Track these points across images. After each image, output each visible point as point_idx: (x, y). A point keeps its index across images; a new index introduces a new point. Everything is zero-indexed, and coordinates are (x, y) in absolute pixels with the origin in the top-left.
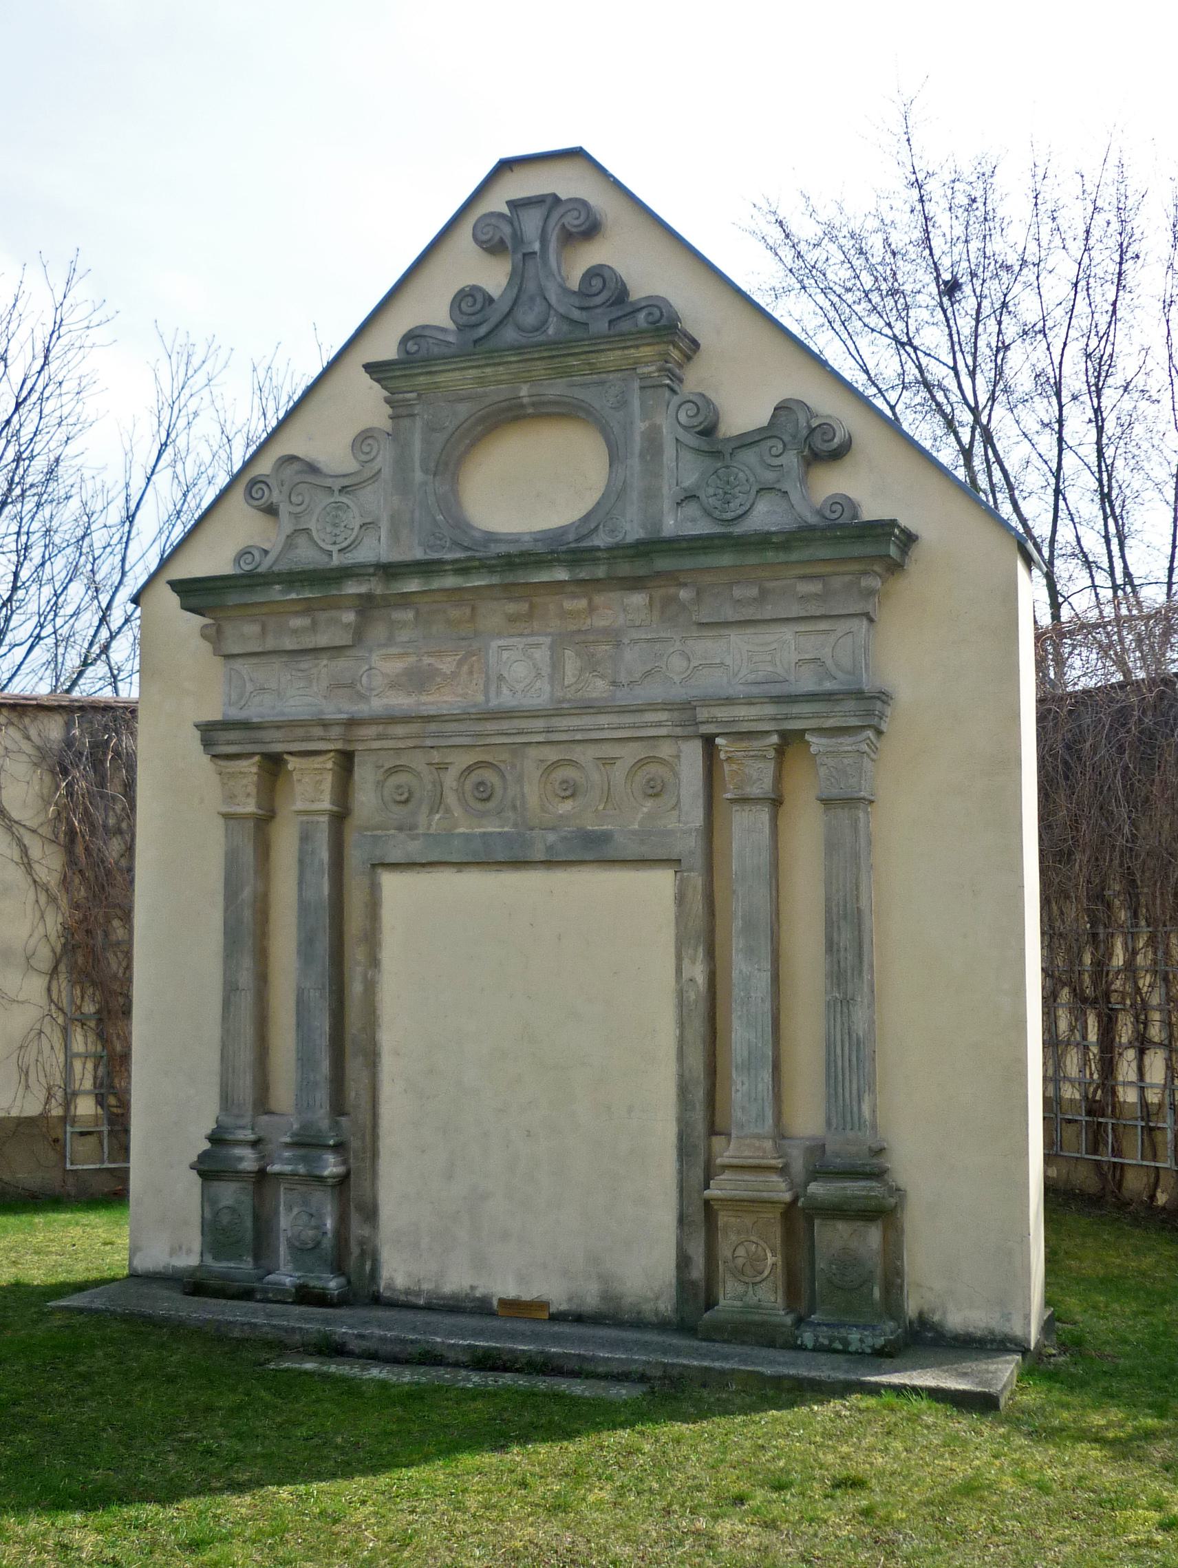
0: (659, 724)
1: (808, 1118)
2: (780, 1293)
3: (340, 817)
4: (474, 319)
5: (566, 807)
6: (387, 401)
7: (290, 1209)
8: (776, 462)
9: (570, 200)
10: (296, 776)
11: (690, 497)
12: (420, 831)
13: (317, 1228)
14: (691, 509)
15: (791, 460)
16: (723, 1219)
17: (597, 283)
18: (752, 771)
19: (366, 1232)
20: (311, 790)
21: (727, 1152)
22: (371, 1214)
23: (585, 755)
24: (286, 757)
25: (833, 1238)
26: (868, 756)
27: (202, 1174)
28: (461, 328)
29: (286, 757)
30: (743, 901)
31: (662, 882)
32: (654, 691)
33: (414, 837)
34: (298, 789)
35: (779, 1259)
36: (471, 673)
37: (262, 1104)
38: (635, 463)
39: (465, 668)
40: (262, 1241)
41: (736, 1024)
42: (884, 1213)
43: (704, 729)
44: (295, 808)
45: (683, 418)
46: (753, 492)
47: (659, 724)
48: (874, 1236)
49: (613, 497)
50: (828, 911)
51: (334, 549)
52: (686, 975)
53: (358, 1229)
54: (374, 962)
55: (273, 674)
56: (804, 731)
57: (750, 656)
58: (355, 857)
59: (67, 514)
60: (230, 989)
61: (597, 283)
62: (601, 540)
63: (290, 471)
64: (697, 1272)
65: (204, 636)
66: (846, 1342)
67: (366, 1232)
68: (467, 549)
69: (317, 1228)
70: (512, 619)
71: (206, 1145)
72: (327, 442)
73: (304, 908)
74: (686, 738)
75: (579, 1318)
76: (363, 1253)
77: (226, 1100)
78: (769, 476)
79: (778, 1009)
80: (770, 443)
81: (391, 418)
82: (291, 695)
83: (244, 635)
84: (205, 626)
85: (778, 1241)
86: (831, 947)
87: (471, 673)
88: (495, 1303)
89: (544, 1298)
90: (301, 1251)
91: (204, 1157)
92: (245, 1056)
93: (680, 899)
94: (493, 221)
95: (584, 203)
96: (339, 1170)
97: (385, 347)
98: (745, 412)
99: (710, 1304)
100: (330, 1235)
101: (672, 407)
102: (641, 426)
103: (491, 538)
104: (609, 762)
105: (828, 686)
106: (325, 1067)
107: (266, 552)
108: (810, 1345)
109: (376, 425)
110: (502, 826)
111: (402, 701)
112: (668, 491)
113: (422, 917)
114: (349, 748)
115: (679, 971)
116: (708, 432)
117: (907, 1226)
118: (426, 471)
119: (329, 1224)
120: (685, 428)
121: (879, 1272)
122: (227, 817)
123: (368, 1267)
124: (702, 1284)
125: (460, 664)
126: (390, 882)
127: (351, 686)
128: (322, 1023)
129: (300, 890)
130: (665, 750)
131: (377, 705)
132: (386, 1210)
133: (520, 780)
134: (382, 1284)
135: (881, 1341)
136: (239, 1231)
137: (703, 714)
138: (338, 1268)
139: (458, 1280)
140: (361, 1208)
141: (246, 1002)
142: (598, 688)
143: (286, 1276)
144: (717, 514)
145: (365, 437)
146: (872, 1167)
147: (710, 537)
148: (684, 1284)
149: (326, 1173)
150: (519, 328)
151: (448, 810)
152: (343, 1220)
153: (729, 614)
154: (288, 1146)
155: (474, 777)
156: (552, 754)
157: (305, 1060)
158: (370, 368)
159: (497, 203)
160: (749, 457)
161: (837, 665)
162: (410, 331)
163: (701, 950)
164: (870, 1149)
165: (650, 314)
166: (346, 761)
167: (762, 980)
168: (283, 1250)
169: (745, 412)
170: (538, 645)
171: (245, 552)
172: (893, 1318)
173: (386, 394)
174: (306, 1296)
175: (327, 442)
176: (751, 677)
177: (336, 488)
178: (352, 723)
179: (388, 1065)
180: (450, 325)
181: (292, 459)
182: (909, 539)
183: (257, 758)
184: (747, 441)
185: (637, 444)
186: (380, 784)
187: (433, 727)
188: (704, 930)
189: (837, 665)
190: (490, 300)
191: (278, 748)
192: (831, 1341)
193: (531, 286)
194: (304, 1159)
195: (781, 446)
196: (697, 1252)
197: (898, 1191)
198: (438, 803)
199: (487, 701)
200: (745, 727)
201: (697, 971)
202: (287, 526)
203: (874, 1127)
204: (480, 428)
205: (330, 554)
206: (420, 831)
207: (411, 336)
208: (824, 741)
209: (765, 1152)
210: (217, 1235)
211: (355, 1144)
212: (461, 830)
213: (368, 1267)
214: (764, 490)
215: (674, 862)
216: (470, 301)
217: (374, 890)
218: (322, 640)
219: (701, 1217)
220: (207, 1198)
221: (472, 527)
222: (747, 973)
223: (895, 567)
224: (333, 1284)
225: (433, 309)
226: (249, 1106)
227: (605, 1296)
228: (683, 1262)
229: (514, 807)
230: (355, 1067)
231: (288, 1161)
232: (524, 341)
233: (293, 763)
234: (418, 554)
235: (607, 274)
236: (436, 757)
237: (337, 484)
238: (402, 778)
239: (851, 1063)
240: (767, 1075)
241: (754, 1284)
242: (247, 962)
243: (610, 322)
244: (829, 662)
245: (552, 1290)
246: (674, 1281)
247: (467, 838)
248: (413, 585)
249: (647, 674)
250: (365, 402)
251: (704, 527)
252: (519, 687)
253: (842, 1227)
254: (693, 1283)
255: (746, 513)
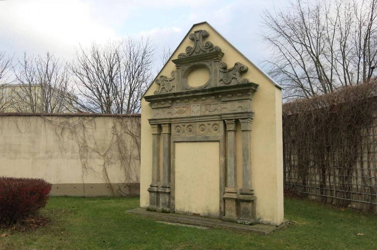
0: (216, 118)
1: (240, 186)
2: (235, 214)
3: (170, 134)
4: (189, 52)
5: (202, 132)
6: (176, 66)
7: (162, 197)
8: (235, 73)
9: (204, 30)
10: (163, 128)
11: (222, 80)
12: (181, 136)
13: (165, 200)
14: (222, 82)
15: (237, 73)
16: (226, 201)
17: (207, 44)
18: (231, 127)
19: (173, 201)
20: (165, 130)
21: (228, 190)
22: (174, 199)
23: (205, 123)
24: (239, 120)
25: (243, 205)
26: (249, 123)
27: (149, 191)
28: (187, 53)
29: (239, 120)
30: (230, 146)
31: (217, 144)
32: (216, 113)
33: (180, 137)
34: (163, 129)
35: (235, 208)
36: (188, 110)
37: (158, 180)
38: (213, 75)
39: (188, 109)
40: (158, 204)
41: (228, 168)
42: (252, 201)
43: (223, 119)
44: (163, 132)
45: (220, 67)
46: (231, 79)
47: (216, 118)
48: (250, 205)
49: (210, 80)
50: (243, 149)
51: (168, 90)
52: (221, 160)
53: (172, 201)
54: (174, 157)
55: (160, 111)
56: (238, 119)
57: (230, 107)
58: (172, 142)
59: (86, 202)
60: (153, 162)
61: (207, 44)
62: (207, 88)
63: (162, 79)
64: (222, 210)
65: (150, 105)
66: (245, 222)
67: (173, 201)
68: (188, 90)
69: (165, 200)
70: (194, 101)
71: (150, 187)
72: (167, 73)
73: (164, 148)
74: (221, 120)
75: (205, 217)
76: (172, 205)
77: (153, 180)
78: (234, 76)
79: (236, 166)
80: (234, 70)
81: (177, 69)
82: (162, 114)
83: (155, 105)
84: (150, 104)
85: (235, 205)
86: (243, 155)
87: (188, 110)
88: (192, 214)
89: (199, 213)
90: (164, 204)
91: (149, 189)
92: (156, 173)
93: (220, 147)
94: (192, 35)
95: (206, 31)
96: (169, 191)
97: (176, 57)
98: (231, 65)
99: (224, 215)
100: (167, 202)
101: (219, 65)
102: (214, 68)
103: (192, 88)
104: (209, 124)
105: (243, 111)
106: (167, 174)
107: (159, 91)
108: (239, 222)
109: (174, 70)
110: (193, 135)
111: (178, 115)
112: (218, 79)
113: (182, 151)
114: (170, 123)
115: (220, 159)
116: (225, 68)
117: (257, 203)
118: (182, 77)
119: (167, 200)
120: (221, 68)
121: (251, 211)
122: (153, 134)
123: (173, 207)
124: (223, 212)
125: (187, 109)
126: (177, 145)
127: (171, 113)
128: (167, 167)
129: (163, 146)
130: (217, 122)
131: (174, 116)
132: (176, 198)
133: (196, 128)
134: (175, 210)
135: (250, 223)
136: (155, 201)
137: (223, 116)
138: (169, 206)
139: (187, 209)
140: (172, 197)
141: (156, 163)
142: (207, 113)
143: (160, 208)
144: (226, 82)
145: (173, 72)
146: (251, 193)
147: (224, 87)
148: (220, 212)
149: (167, 192)
150: (196, 53)
151: (185, 133)
152: (170, 199)
153: (227, 99)
154: (162, 187)
155: (189, 127)
156: (176, 125)
157: (164, 173)
158: (172, 61)
159: (193, 32)
160: (231, 73)
161: (244, 107)
162: (182, 53)
163: (223, 156)
164: (250, 190)
165: (216, 49)
166: (170, 125)
167: (233, 160)
168: (161, 204)
169: (231, 65)
170: (198, 105)
171: (156, 92)
172: (253, 219)
173: (175, 65)
174: (164, 212)
175: (167, 73)
176: (231, 110)
177: (168, 81)
178: (171, 119)
179: (176, 174)
180: (186, 53)
181: (162, 76)
182: (256, 86)
183: (234, 120)
184: (230, 70)
185: (213, 71)
186: (175, 128)
187: (183, 119)
188: (224, 153)
189: (244, 107)
190: (192, 48)
191: (160, 123)
192: (242, 222)
193: (198, 46)
194: (163, 189)
195: (236, 70)
196: (223, 208)
197: (256, 198)
198: (184, 132)
199: (191, 115)
200: (229, 118)
201: (223, 159)
202: (162, 87)
203: (251, 186)
204: (187, 73)
205: (168, 91)
206: (181, 136)
207: (180, 55)
208: (242, 120)
209: (232, 190)
210: (152, 202)
211: (171, 187)
212: (187, 136)
213: (173, 207)
214: (233, 78)
215: (218, 141)
216: (188, 48)
217: (174, 145)
218: (166, 105)
219: (224, 200)
220: (150, 196)
221: (189, 86)
222: (231, 160)
223: (255, 91)
224: (168, 209)
225: (183, 50)
226: (156, 181)
227: (208, 214)
228: (220, 208)
229: (195, 132)
230: (172, 176)
231: (161, 190)
232: (197, 55)
233: (241, 121)
234: (180, 91)
235: (209, 43)
236: (183, 124)
237: (168, 80)
238: (178, 128)
239: (247, 175)
240: (233, 177)
241: (231, 212)
242: (156, 157)
243: (210, 51)
244: (243, 107)
245: (200, 211)
246: (219, 211)
247: (188, 137)
248: (179, 96)
249: (215, 110)
250: (172, 66)
251: (223, 85)
252: (196, 112)
253: (245, 203)
254: (222, 212)
255: (231, 82)
